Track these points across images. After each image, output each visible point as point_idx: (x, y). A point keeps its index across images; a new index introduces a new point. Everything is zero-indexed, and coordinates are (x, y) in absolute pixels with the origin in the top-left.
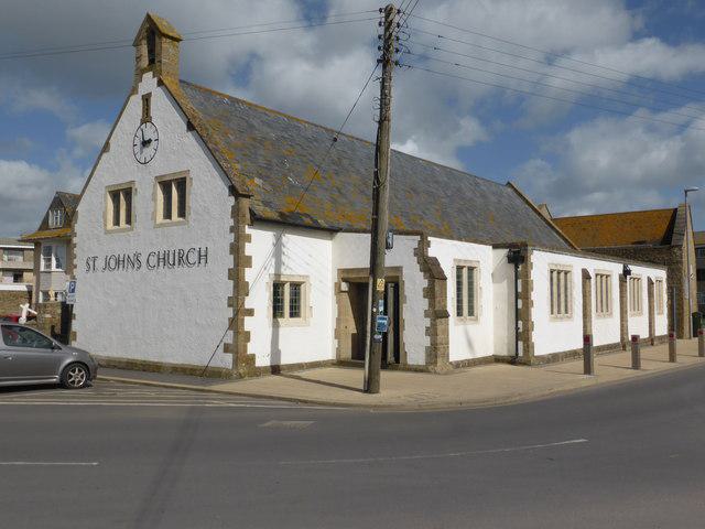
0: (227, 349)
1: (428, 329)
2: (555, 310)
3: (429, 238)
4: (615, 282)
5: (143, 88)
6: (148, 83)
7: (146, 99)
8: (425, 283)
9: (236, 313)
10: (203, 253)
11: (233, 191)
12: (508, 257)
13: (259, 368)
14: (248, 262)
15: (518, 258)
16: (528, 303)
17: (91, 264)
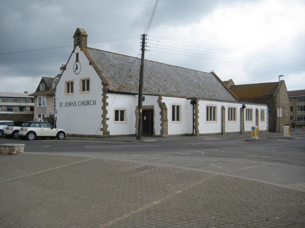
0: (101, 130)
1: (161, 124)
3: (162, 97)
5: (76, 51)
6: (78, 49)
7: (77, 54)
8: (160, 110)
9: (104, 119)
10: (95, 102)
11: (103, 83)
12: (191, 102)
14: (107, 104)
15: (194, 102)
17: (61, 105)
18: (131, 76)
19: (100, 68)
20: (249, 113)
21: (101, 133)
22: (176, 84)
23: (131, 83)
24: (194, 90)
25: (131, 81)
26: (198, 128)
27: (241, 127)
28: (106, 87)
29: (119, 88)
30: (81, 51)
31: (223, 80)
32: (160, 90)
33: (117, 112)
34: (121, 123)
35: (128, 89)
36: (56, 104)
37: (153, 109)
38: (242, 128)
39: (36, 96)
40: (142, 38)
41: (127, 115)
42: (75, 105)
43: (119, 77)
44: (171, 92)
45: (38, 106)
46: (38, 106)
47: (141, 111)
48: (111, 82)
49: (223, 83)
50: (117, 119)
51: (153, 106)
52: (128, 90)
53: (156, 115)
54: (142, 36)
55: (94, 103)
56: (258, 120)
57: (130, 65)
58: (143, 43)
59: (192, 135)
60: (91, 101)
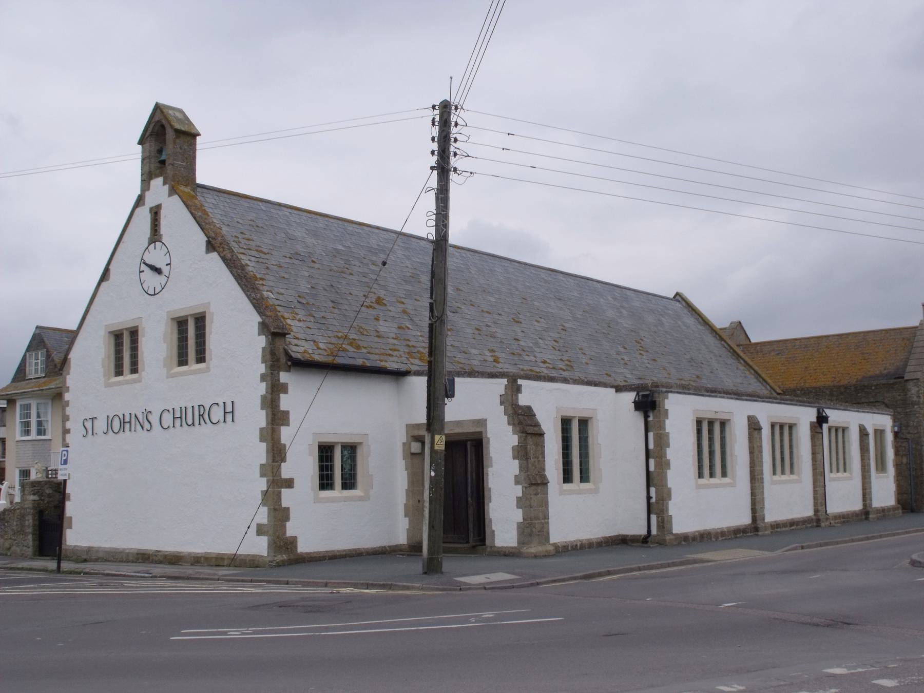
0: (260, 531)
2: (706, 471)
3: (520, 382)
4: (804, 434)
5: (150, 201)
7: (156, 213)
8: (514, 440)
10: (229, 409)
11: (264, 328)
12: (635, 402)
13: (301, 554)
16: (664, 464)
17: (89, 430)
18: (379, 301)
19: (252, 267)
20: (837, 442)
21: (259, 546)
22: (559, 336)
23: (381, 329)
24: (626, 358)
25: (381, 322)
26: (667, 510)
27: (815, 498)
28: (280, 344)
29: (331, 346)
30: (170, 195)
31: (720, 322)
32: (502, 356)
33: (325, 452)
34: (346, 499)
35: (373, 351)
36: (68, 425)
37: (481, 433)
38: (819, 501)
39: (11, 402)
40: (437, 118)
41: (367, 464)
42: (147, 426)
43: (331, 305)
44: (542, 365)
45: (19, 437)
46: (19, 437)
47: (440, 443)
48: (301, 324)
49: (721, 333)
50: (326, 482)
51: (482, 422)
52: (371, 357)
53: (494, 459)
54: (437, 112)
55: (229, 417)
56: (869, 471)
57: (374, 258)
58: (444, 141)
59: (645, 540)
60: (215, 408)
